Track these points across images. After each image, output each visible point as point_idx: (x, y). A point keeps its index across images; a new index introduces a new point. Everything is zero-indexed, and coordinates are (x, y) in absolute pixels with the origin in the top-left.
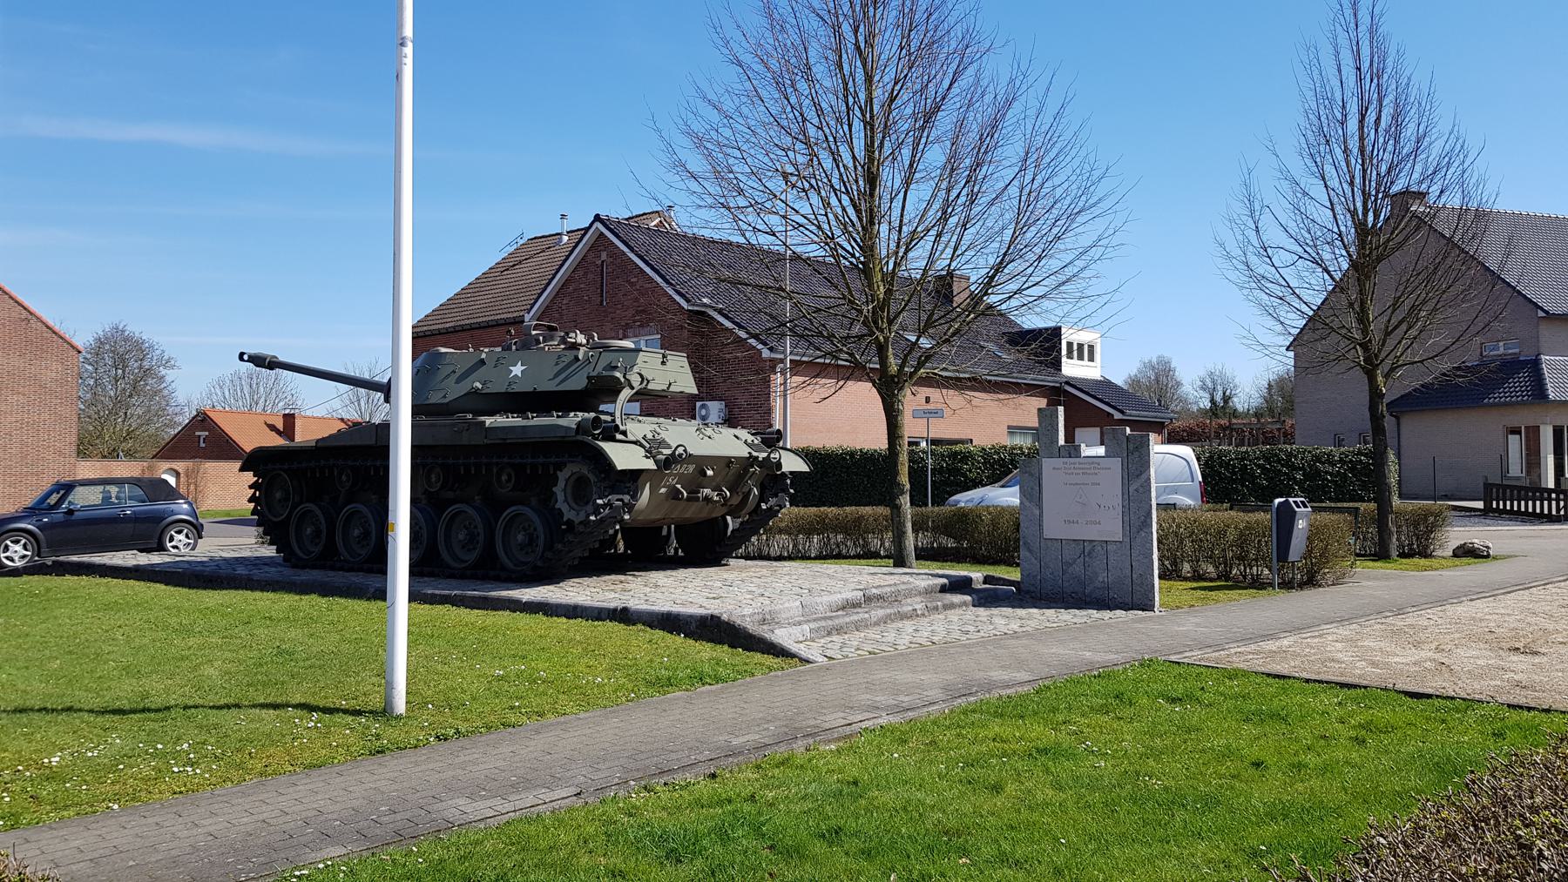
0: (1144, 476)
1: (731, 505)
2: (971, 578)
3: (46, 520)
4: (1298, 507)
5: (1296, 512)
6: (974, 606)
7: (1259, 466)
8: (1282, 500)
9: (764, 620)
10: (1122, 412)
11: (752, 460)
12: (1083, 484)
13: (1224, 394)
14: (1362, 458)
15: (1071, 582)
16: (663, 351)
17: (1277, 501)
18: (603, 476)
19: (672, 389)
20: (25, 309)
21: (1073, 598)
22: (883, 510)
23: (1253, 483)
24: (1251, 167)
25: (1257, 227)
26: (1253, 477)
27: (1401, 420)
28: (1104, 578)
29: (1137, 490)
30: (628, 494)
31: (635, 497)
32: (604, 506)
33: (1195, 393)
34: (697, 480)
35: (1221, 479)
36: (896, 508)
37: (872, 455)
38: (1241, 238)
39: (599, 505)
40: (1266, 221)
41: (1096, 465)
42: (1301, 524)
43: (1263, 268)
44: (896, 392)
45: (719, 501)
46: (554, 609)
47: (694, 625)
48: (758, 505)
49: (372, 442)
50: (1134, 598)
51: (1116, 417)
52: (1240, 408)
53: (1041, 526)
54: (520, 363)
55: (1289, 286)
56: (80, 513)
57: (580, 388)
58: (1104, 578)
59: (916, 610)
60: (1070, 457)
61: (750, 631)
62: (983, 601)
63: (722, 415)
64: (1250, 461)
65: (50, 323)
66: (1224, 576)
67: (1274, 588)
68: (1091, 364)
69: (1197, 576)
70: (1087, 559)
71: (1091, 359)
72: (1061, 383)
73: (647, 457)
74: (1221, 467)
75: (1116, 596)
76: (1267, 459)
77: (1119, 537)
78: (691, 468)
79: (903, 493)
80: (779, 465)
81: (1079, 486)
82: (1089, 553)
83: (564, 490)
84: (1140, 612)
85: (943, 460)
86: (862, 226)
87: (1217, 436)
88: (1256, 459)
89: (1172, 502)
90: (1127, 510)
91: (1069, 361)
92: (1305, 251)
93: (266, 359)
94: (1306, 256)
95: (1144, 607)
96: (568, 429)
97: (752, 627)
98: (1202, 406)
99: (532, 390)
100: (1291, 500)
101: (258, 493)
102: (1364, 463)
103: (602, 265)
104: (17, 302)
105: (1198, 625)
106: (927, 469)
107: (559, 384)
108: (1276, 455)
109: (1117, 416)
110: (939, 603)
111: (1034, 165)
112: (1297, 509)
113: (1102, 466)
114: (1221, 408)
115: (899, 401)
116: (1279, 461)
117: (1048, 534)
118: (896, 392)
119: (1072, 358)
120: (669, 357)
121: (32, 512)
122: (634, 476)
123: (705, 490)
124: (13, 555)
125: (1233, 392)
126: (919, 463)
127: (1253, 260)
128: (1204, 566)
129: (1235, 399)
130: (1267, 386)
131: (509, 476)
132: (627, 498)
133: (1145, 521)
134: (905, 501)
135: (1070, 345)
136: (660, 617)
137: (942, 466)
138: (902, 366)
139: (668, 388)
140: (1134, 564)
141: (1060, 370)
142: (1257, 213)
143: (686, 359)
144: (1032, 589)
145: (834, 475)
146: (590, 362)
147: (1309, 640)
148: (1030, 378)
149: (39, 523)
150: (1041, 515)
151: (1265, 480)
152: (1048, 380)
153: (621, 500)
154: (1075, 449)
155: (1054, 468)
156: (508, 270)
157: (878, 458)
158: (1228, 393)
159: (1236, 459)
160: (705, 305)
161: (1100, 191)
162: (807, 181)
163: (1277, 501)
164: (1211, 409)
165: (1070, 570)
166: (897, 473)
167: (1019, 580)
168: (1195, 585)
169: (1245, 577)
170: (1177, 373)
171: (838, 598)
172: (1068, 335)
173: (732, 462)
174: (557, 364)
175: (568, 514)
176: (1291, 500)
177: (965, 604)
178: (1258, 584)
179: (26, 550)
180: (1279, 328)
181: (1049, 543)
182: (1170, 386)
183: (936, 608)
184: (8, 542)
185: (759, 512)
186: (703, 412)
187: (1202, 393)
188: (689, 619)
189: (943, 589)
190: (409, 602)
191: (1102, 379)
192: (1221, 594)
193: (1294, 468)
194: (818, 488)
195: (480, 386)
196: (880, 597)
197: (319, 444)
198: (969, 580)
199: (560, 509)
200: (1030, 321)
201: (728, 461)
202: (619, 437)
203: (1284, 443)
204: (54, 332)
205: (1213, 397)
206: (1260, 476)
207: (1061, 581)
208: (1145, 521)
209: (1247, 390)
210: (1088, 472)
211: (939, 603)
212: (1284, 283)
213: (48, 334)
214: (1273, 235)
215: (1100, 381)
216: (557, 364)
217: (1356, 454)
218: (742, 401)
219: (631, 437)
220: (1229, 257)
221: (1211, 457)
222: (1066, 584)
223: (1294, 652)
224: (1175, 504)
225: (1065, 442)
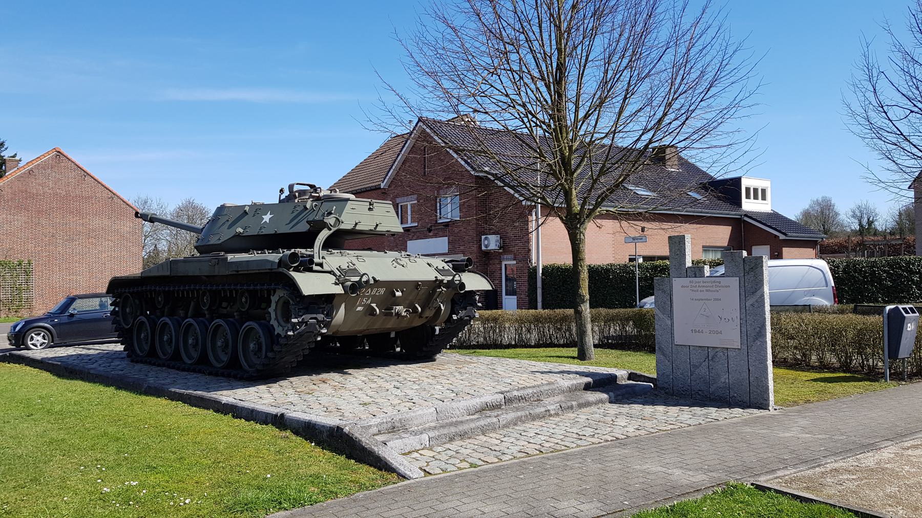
0: (759, 293)
1: (427, 317)
2: (616, 376)
3: (56, 320)
4: (907, 312)
5: (905, 317)
6: (610, 402)
7: (885, 271)
8: (892, 307)
9: (394, 428)
11: (438, 283)
12: (707, 300)
13: (868, 220)
16: (370, 200)
17: (888, 308)
18: (298, 299)
19: (358, 228)
20: (111, 191)
21: (699, 395)
22: (570, 311)
23: (880, 284)
24: (869, 41)
25: (875, 89)
26: (880, 280)
28: (725, 379)
30: (323, 314)
31: (330, 314)
32: (299, 323)
33: (848, 220)
34: (388, 301)
35: (855, 281)
36: (578, 313)
38: (863, 99)
39: (295, 323)
40: (882, 85)
41: (717, 284)
42: (910, 327)
43: (878, 120)
44: (578, 226)
45: (406, 316)
46: (240, 410)
47: (325, 434)
48: (450, 317)
49: (168, 273)
51: (781, 238)
52: (879, 228)
53: (672, 334)
54: (269, 213)
55: (902, 134)
56: (78, 316)
57: (350, 228)
58: (725, 379)
59: (549, 410)
60: (695, 277)
61: (364, 444)
62: (620, 397)
63: (498, 244)
64: (878, 268)
65: (126, 199)
66: (845, 367)
67: (886, 381)
69: (823, 366)
71: (764, 198)
72: (741, 216)
73: (336, 284)
74: (855, 272)
76: (891, 267)
77: (737, 345)
78: (382, 291)
79: (583, 302)
80: (462, 285)
81: (704, 301)
83: (275, 310)
84: (755, 411)
85: (647, 271)
86: (552, 101)
87: (854, 250)
88: (882, 266)
89: (808, 304)
92: (915, 106)
93: (148, 216)
94: (916, 109)
95: (760, 406)
96: (272, 262)
97: (366, 440)
98: (853, 228)
99: (274, 232)
100: (900, 307)
101: (117, 309)
103: (425, 149)
104: (105, 187)
105: (804, 429)
106: (636, 279)
107: (292, 227)
108: (898, 263)
109: (782, 237)
110: (574, 403)
111: (674, 45)
112: (905, 315)
113: (722, 284)
114: (867, 228)
115: (581, 232)
116: (900, 268)
117: (678, 341)
118: (578, 226)
119: (750, 199)
120: (375, 205)
121: (49, 317)
122: (328, 300)
123: (398, 307)
124: (36, 343)
125: (875, 219)
126: (630, 274)
127: (872, 114)
128: (828, 355)
129: (876, 223)
130: (898, 214)
131: (246, 298)
132: (321, 317)
133: (760, 332)
134: (586, 308)
135: (748, 190)
136: (303, 425)
137: (647, 276)
138: (583, 206)
139: (375, 228)
140: (750, 368)
142: (875, 79)
143: (391, 206)
144: (666, 385)
146: (314, 210)
147: (910, 452)
148: (717, 213)
149: (52, 323)
151: (889, 281)
152: (733, 214)
153: (315, 318)
154: (700, 270)
155: (682, 287)
156: (378, 157)
157: (601, 271)
158: (871, 219)
159: (867, 267)
160: (486, 172)
161: (734, 62)
162: (517, 73)
163: (888, 308)
164: (860, 230)
166: (579, 287)
167: (656, 377)
168: (818, 376)
169: (863, 367)
170: (835, 207)
171: (477, 402)
172: (745, 183)
173: (419, 285)
174: (293, 212)
175: (278, 330)
176: (900, 307)
177: (601, 401)
178: (873, 375)
179: (45, 339)
180: (895, 167)
181: (679, 348)
182: (831, 216)
183: (571, 407)
184: (33, 335)
185: (452, 321)
186: (486, 242)
187: (853, 220)
188: (322, 429)
189: (587, 387)
190: (782, 258)
191: (772, 212)
192: (837, 387)
193: (911, 272)
194: (561, 291)
195: (242, 231)
196: (520, 399)
197: (143, 275)
198: (613, 378)
199: (272, 325)
200: (719, 172)
201: (416, 285)
202: (315, 268)
203: (905, 254)
204: (128, 205)
205: (861, 222)
206: (886, 278)
207: (689, 380)
208: (760, 332)
209: (884, 217)
210: (711, 289)
211: (574, 403)
212: (898, 133)
213: (124, 206)
214: (888, 95)
215: (771, 214)
216: (293, 212)
218: (511, 235)
219: (326, 268)
220: (853, 114)
221: (847, 266)
223: (893, 470)
224: (809, 305)
225: (748, 255)
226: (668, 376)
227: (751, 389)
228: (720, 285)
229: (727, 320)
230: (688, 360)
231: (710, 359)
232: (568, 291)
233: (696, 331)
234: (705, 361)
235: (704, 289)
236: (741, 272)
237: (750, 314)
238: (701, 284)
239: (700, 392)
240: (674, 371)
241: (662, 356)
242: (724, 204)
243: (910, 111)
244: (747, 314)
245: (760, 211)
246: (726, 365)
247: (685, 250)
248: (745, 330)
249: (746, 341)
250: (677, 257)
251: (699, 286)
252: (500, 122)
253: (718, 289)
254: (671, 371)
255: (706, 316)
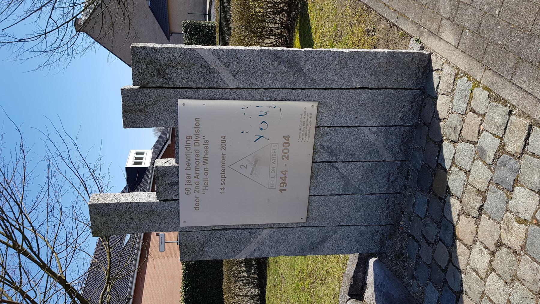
10: (167, 140)
14: (188, 30)
15: (373, 181)
27: (174, 32)
29: (235, 75)
37: (186, 274)
41: (192, 142)
50: (407, 86)
51: (170, 143)
60: (177, 184)
68: (145, 154)
70: (341, 158)
71: (143, 154)
75: (400, 115)
82: (332, 154)
90: (267, 93)
91: (143, 163)
102: (191, 30)
113: (192, 132)
133: (288, 62)
135: (135, 163)
141: (147, 167)
144: (377, 237)
145: (197, 296)
150: (270, 227)
165: (355, 183)
172: (130, 164)
207: (370, 197)
217: (187, 33)
222: (376, 190)
226: (361, 234)
227: (391, 86)
228: (194, 137)
229: (264, 126)
230: (335, 198)
231: (334, 159)
232: (204, 298)
233: (284, 184)
234: (337, 169)
235: (202, 168)
236: (167, 95)
237: (254, 80)
238: (192, 173)
239: (392, 178)
240: (354, 223)
241: (326, 245)
242: (145, 178)
243: (50, 19)
244: (253, 86)
245: (152, 156)
246: (347, 130)
247: (123, 204)
248: (284, 91)
249: (304, 92)
250: (136, 220)
251: (196, 177)
252: (260, 137)
253: (202, 141)
254: (353, 228)
255: (255, 164)
